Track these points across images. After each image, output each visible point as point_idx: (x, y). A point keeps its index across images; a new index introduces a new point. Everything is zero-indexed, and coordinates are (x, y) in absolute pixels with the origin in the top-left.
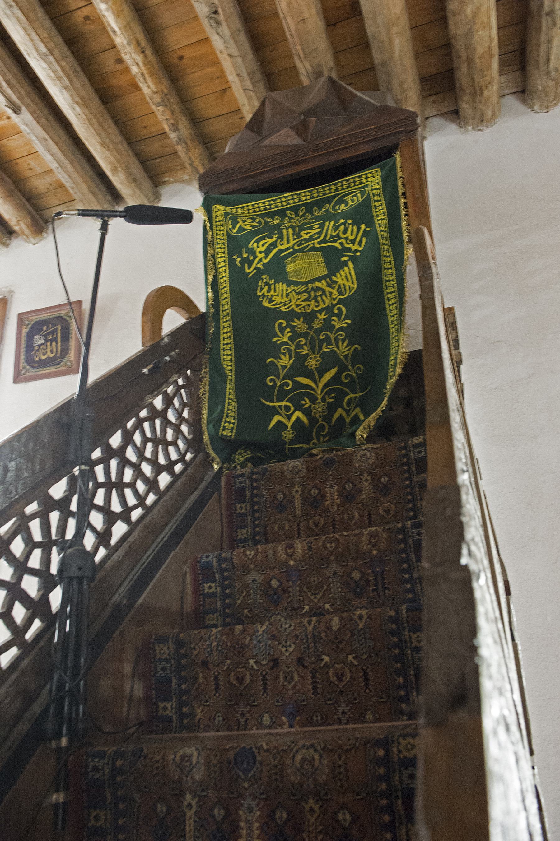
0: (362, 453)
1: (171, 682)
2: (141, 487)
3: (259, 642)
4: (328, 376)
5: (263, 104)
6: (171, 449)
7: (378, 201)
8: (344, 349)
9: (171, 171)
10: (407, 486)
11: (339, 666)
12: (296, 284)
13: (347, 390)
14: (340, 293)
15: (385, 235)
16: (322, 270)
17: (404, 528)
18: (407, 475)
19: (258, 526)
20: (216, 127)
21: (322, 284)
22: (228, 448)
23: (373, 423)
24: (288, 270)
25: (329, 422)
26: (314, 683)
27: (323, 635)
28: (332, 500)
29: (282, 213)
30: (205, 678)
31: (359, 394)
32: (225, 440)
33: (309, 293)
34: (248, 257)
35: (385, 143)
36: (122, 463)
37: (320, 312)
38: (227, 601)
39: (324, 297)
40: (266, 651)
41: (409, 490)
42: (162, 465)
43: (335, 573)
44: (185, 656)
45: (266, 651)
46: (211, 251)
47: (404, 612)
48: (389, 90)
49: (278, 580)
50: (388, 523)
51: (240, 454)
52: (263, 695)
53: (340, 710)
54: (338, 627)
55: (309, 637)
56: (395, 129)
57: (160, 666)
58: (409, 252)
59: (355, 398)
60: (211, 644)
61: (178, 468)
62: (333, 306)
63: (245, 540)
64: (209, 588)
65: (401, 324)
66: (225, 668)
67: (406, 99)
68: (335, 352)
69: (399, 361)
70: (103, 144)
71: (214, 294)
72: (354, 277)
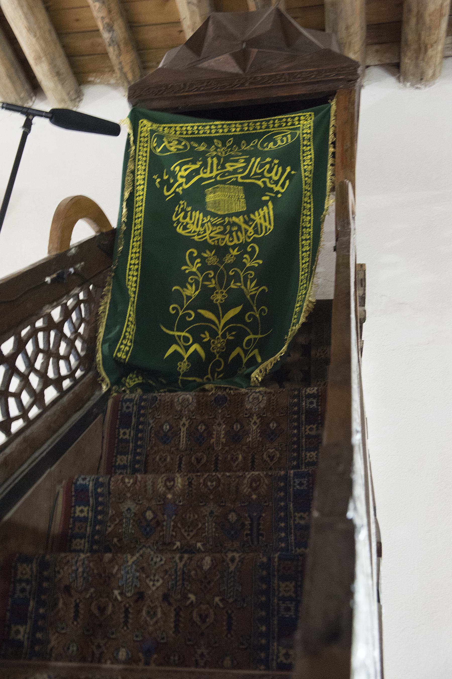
0: (256, 395)
1: (29, 605)
2: (26, 398)
3: (128, 573)
4: (232, 313)
5: (206, 24)
6: (62, 363)
7: (307, 146)
8: (251, 289)
9: (99, 71)
10: (294, 435)
11: (204, 607)
12: (214, 215)
13: (248, 330)
14: (256, 232)
15: (309, 181)
16: (241, 206)
17: (285, 478)
18: (296, 424)
19: (139, 454)
20: (152, 35)
21: (240, 220)
22: (120, 370)
23: (270, 367)
24: (207, 200)
25: (226, 361)
26: (177, 621)
27: (193, 573)
28: (218, 437)
29: (209, 141)
30: (65, 604)
31: (259, 336)
32: (118, 361)
33: (225, 227)
34: (168, 179)
35: (323, 88)
36: (10, 371)
37: (234, 247)
38: (97, 528)
39: (239, 233)
40: (132, 584)
41: (295, 439)
42: (51, 379)
43: (212, 512)
44: (48, 579)
45: (132, 584)
46: (131, 166)
47: (276, 560)
48: (335, 31)
49: (153, 512)
50: (271, 469)
51: (131, 378)
52: (123, 628)
53: (199, 652)
54: (208, 567)
55: (179, 573)
56: (333, 76)
57: (19, 587)
58: (330, 203)
59: (255, 339)
60: (77, 569)
61: (66, 383)
62: (247, 244)
63: (124, 467)
64: (81, 511)
65: (311, 274)
66: (88, 596)
67: (350, 43)
68: (243, 290)
69: (304, 310)
70: (30, 29)
71: (128, 211)
72: (272, 218)
